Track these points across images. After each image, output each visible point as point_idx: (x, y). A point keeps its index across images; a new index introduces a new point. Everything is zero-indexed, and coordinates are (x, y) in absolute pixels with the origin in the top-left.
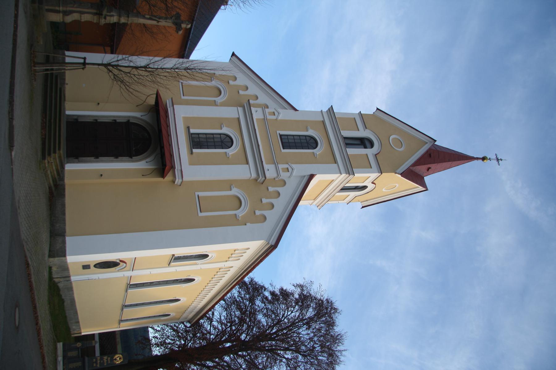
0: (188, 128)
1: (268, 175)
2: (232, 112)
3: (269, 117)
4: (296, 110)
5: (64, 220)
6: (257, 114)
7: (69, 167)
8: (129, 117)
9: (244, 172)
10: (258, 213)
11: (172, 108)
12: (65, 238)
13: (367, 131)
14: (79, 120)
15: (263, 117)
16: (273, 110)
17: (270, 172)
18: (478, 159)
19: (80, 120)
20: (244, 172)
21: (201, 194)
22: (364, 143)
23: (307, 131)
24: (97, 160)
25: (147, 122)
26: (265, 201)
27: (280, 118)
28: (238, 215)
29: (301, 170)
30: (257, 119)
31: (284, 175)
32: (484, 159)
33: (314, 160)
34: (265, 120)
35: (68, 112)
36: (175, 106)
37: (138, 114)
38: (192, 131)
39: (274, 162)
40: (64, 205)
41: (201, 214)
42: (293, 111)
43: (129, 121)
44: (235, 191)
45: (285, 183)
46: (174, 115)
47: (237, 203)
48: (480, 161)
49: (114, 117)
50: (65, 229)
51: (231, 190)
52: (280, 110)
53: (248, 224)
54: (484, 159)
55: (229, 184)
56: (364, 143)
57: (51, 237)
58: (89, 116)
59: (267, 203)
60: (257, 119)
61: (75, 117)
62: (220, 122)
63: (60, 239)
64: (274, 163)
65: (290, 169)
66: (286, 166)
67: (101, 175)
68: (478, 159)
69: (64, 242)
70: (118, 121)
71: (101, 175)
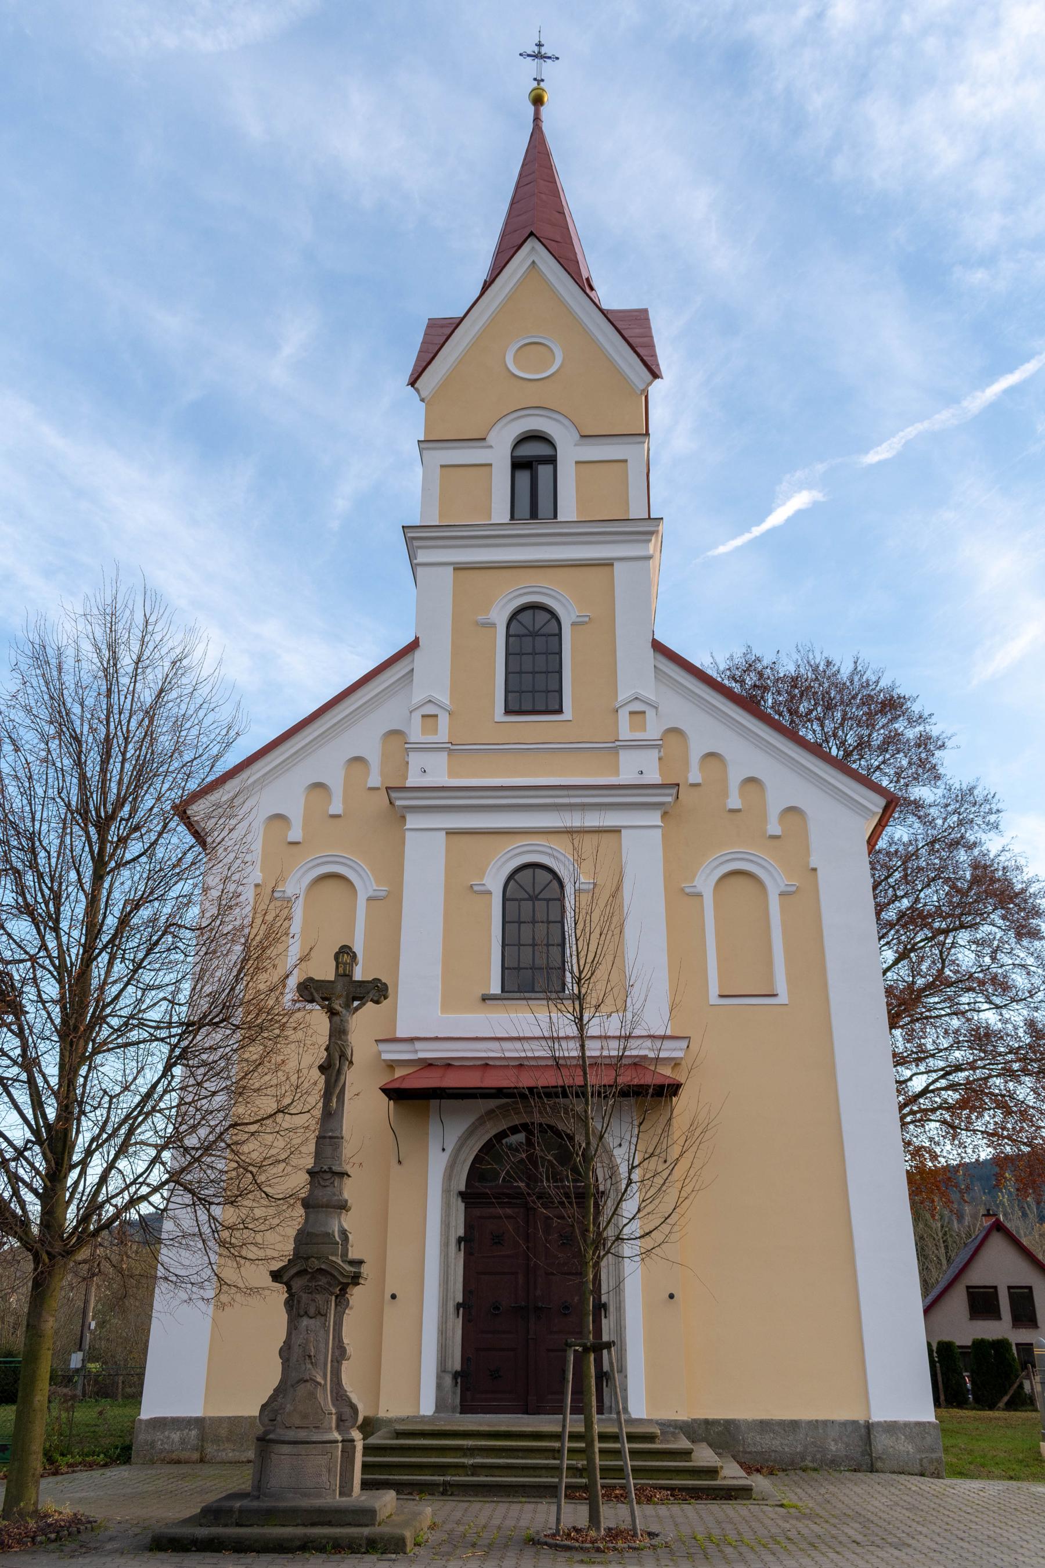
0: (485, 998)
1: (653, 776)
2: (425, 851)
3: (443, 734)
4: (414, 646)
5: (814, 1425)
6: (431, 770)
7: (642, 1400)
8: (446, 1191)
9: (643, 848)
10: (774, 827)
11: (418, 1045)
12: (879, 1424)
13: (491, 439)
14: (458, 1367)
15: (445, 754)
16: (417, 717)
17: (638, 767)
18: (537, 119)
19: (456, 1363)
20: (643, 848)
21: (714, 990)
22: (533, 460)
23: (493, 625)
24: (612, 1309)
25: (470, 1132)
26: (734, 801)
27: (444, 698)
28: (371, 893)
29: (636, 676)
30: (451, 774)
31: (653, 730)
32: (538, 101)
33: (603, 624)
34: (452, 749)
35: (427, 1407)
36: (400, 1034)
37: (437, 1163)
38: (496, 989)
39: (614, 748)
40: (764, 1426)
41: (783, 998)
42: (418, 654)
43: (461, 1194)
44: (705, 882)
45: (675, 731)
46: (437, 1039)
47: (330, 885)
48: (544, 110)
49: (445, 1245)
50: (844, 1424)
51: (699, 895)
52: (418, 696)
53: (813, 862)
54: (538, 101)
55: (680, 897)
56: (533, 460)
57: (872, 1470)
58: (443, 1332)
59: (741, 794)
60: (451, 774)
61: (448, 1380)
62: (461, 891)
63: (882, 1442)
64: (615, 750)
65: (637, 707)
66: (624, 716)
67: (671, 1296)
68: (537, 119)
69: (892, 1427)
70: (461, 1232)
71: (671, 1296)
